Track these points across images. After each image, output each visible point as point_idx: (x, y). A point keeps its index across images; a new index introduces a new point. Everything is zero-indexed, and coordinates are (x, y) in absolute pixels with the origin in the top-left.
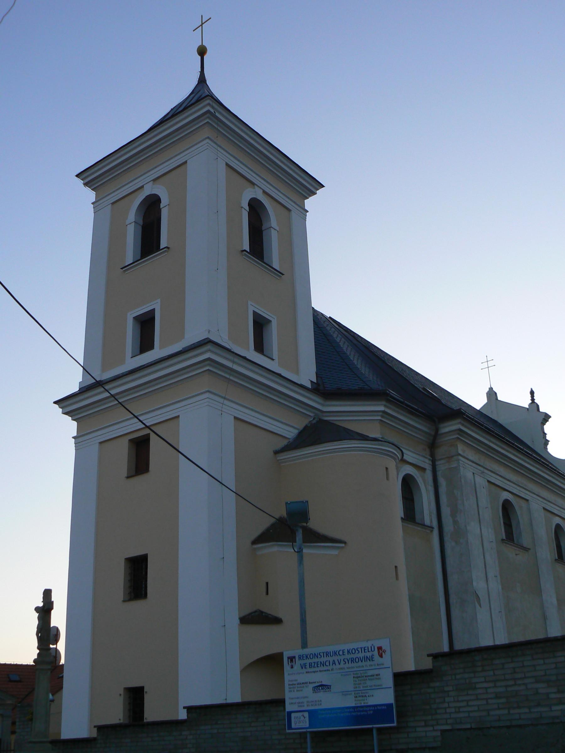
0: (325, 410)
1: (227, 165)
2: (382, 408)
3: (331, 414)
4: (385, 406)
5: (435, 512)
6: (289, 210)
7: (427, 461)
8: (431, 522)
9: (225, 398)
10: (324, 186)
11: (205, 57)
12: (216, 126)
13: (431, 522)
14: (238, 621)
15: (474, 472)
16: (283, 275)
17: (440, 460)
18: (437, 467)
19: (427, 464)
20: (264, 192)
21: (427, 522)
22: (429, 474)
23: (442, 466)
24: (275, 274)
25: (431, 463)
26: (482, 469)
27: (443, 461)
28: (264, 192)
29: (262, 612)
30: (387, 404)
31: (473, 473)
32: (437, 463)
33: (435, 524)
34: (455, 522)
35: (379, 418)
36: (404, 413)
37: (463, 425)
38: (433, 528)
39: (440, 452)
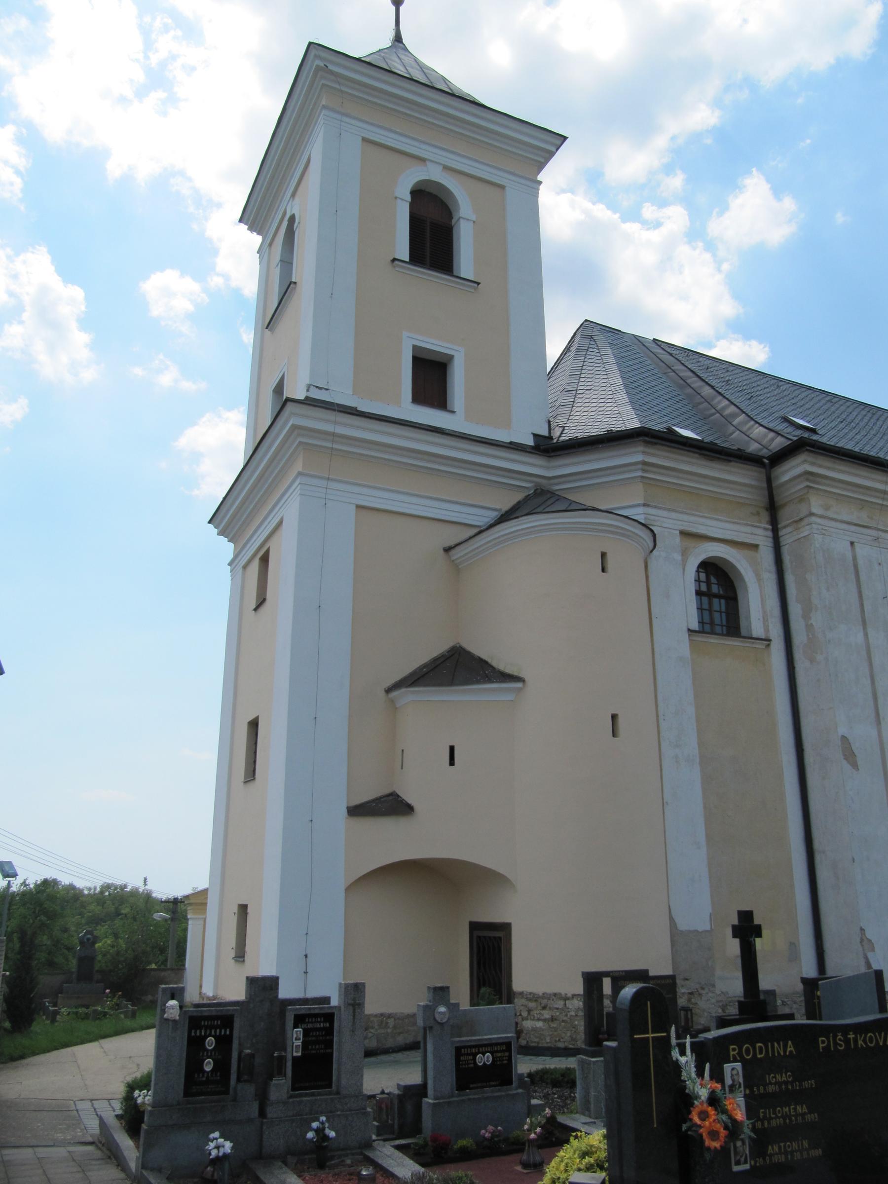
0: (551, 475)
1: (364, 140)
2: (639, 458)
3: (563, 479)
4: (644, 453)
5: (777, 611)
6: (502, 187)
7: (760, 532)
8: (767, 630)
9: (328, 479)
10: (565, 138)
11: (401, 8)
12: (337, 86)
13: (767, 630)
14: (344, 811)
15: (853, 540)
16: (478, 284)
17: (785, 527)
18: (781, 539)
19: (762, 537)
20: (446, 168)
21: (757, 629)
22: (766, 555)
23: (788, 537)
24: (462, 284)
25: (770, 534)
26: (874, 533)
27: (789, 529)
28: (446, 168)
29: (398, 796)
30: (647, 450)
31: (852, 543)
32: (781, 533)
33: (776, 632)
34: (809, 627)
35: (640, 474)
36: (694, 461)
37: (813, 464)
38: (770, 640)
39: (786, 516)
